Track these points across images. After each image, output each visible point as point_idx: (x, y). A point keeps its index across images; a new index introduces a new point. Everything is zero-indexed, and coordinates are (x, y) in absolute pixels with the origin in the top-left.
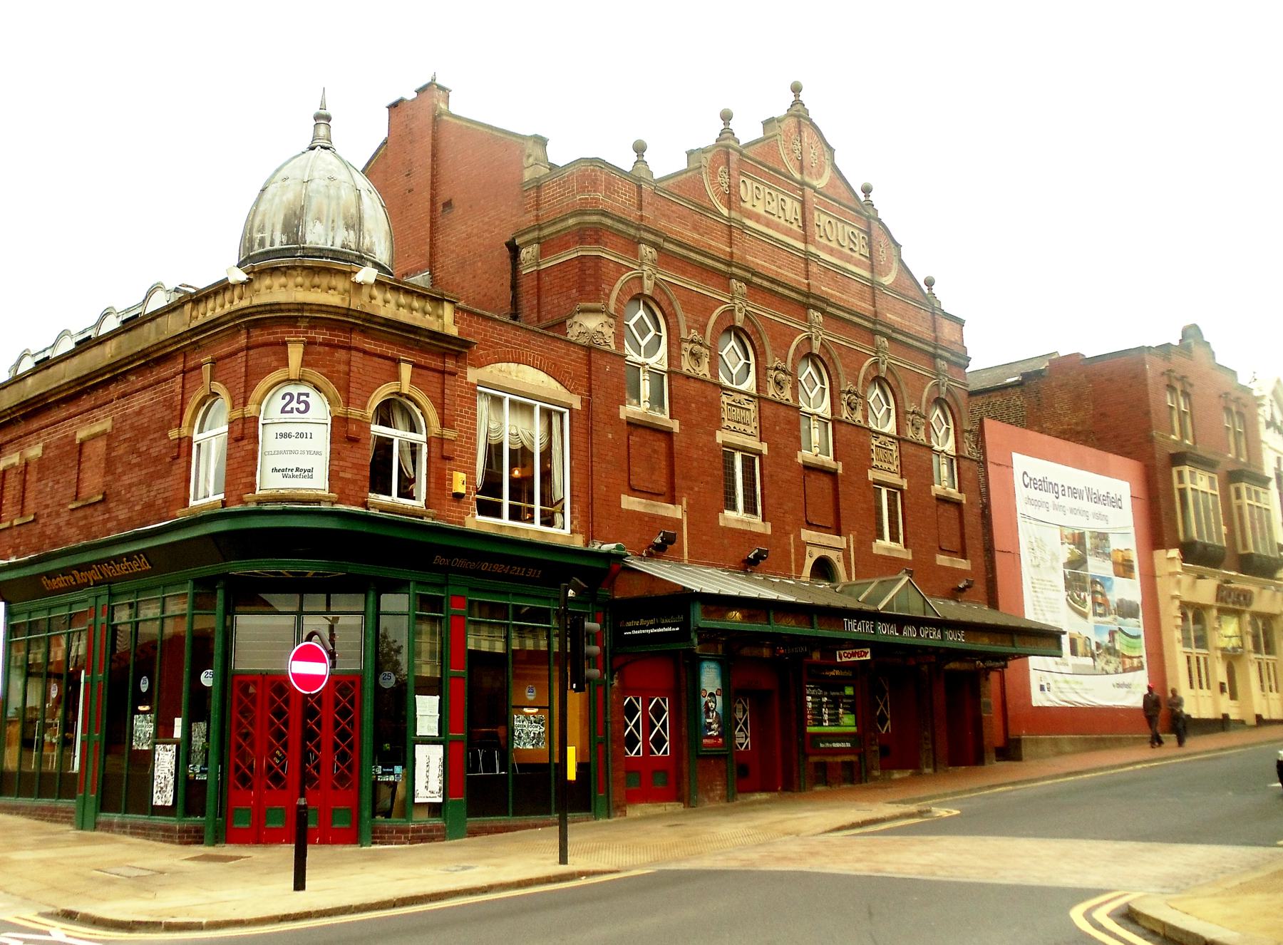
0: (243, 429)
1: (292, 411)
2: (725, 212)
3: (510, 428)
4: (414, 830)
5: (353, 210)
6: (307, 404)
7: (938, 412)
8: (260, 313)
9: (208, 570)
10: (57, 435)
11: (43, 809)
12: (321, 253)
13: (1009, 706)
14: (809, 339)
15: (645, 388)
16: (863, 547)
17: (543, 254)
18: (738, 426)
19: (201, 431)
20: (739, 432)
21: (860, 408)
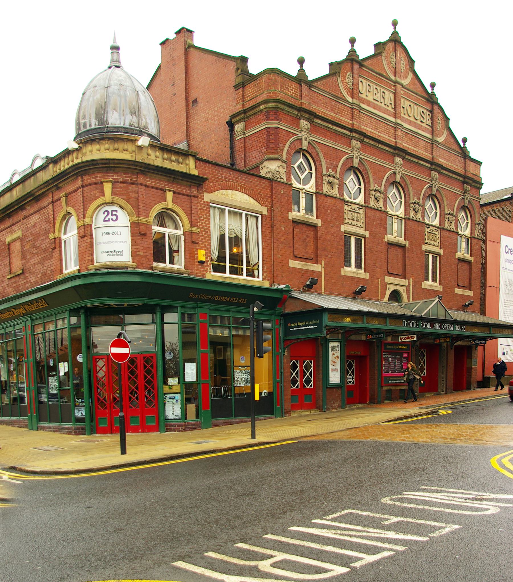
0: (85, 231)
1: (109, 220)
2: (350, 99)
3: (231, 226)
4: (185, 425)
5: (134, 103)
6: (116, 215)
9: (75, 305)
11: (14, 421)
12: (118, 129)
13: (486, 362)
14: (394, 173)
15: (303, 202)
16: (417, 284)
18: (353, 222)
19: (65, 233)
21: (420, 212)
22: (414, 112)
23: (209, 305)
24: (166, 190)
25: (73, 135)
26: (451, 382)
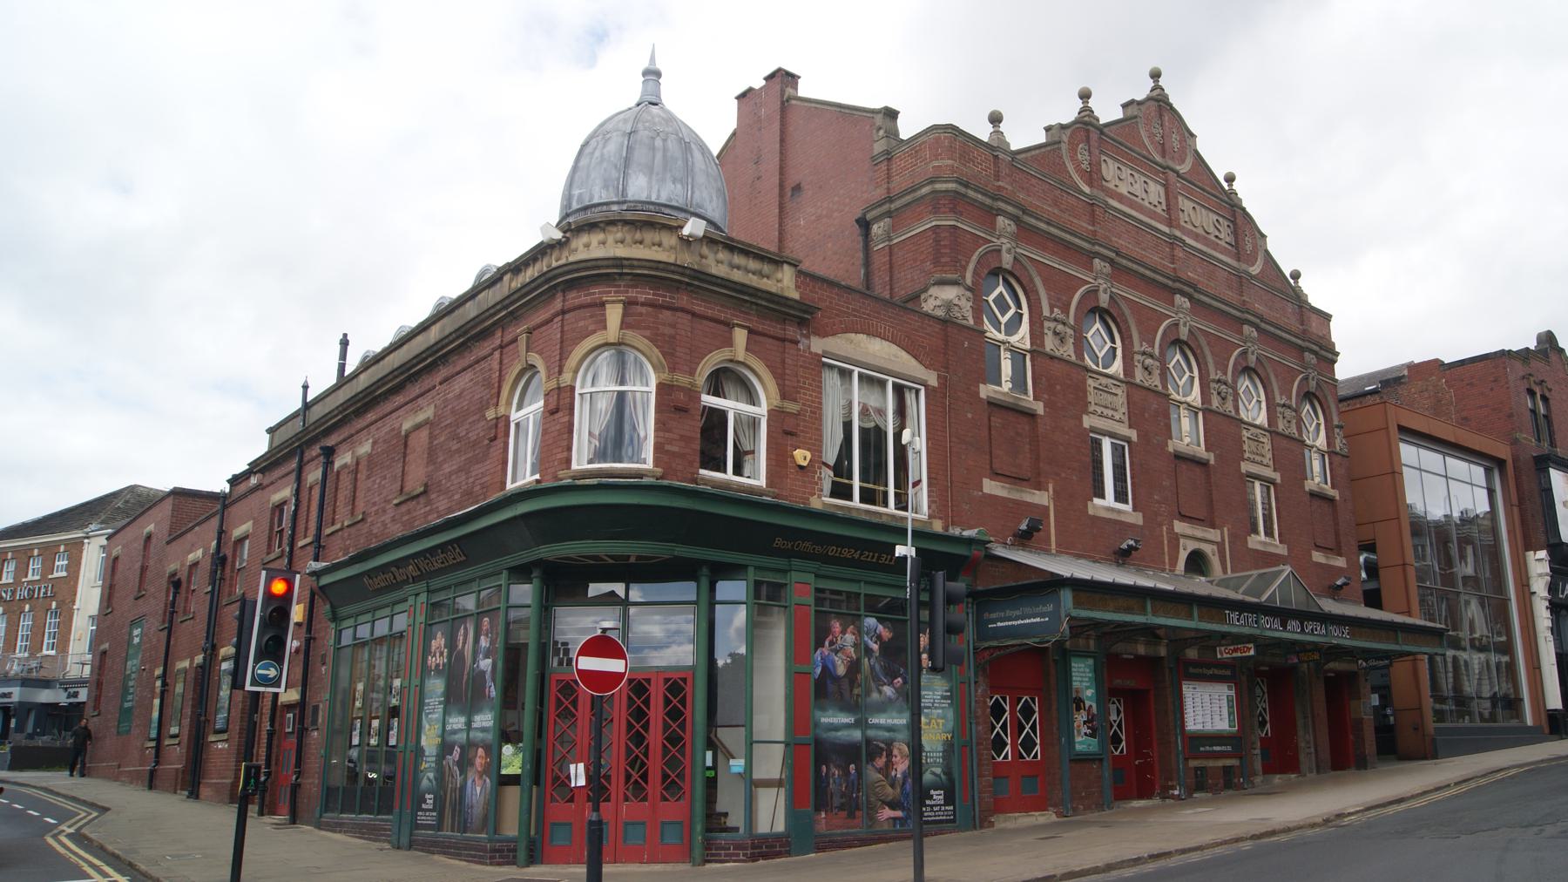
2: (1086, 189)
7: (1308, 407)
8: (577, 270)
10: (384, 429)
11: (364, 826)
15: (1006, 367)
16: (1238, 539)
17: (894, 228)
18: (1106, 412)
19: (520, 407)
20: (1108, 420)
22: (1198, 217)
23: (816, 565)
24: (734, 325)
25: (555, 219)
26: (1326, 755)
